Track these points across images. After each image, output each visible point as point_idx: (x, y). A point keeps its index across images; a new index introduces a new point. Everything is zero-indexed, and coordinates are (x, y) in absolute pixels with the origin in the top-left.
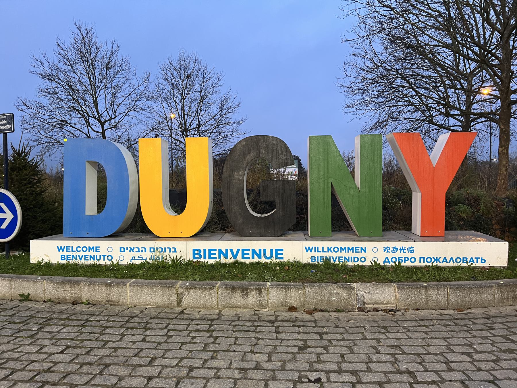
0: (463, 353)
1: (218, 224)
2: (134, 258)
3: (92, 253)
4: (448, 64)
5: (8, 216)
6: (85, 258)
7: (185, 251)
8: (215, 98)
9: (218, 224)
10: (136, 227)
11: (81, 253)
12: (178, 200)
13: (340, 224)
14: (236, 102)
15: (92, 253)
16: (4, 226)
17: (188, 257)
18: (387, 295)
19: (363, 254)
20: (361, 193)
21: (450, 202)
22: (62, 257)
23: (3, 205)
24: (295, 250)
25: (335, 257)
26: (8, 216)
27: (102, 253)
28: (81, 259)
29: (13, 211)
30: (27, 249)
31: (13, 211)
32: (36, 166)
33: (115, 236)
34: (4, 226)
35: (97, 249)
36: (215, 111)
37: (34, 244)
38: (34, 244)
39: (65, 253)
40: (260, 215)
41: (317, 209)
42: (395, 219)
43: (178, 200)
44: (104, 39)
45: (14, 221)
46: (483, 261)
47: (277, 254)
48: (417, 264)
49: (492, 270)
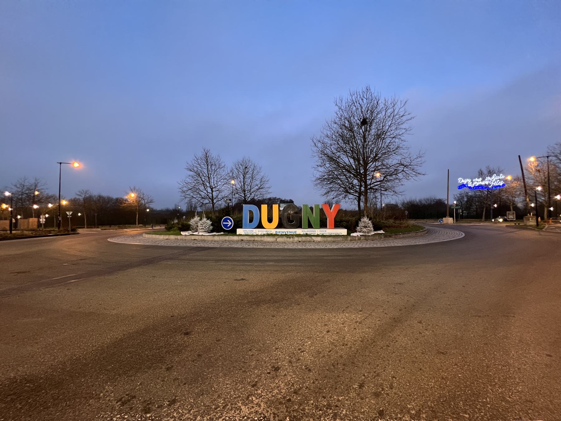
1: (280, 226)
4: (268, 266)
5: (230, 223)
7: (274, 231)
8: (258, 177)
9: (280, 226)
10: (260, 226)
12: (270, 220)
13: (310, 226)
14: (268, 179)
17: (274, 233)
18: (319, 239)
20: (315, 217)
21: (335, 221)
24: (299, 231)
25: (309, 233)
26: (230, 223)
31: (231, 222)
33: (255, 228)
36: (258, 182)
37: (238, 230)
38: (238, 230)
41: (304, 222)
42: (323, 225)
43: (270, 220)
44: (213, 154)
45: (231, 225)
49: (343, 236)
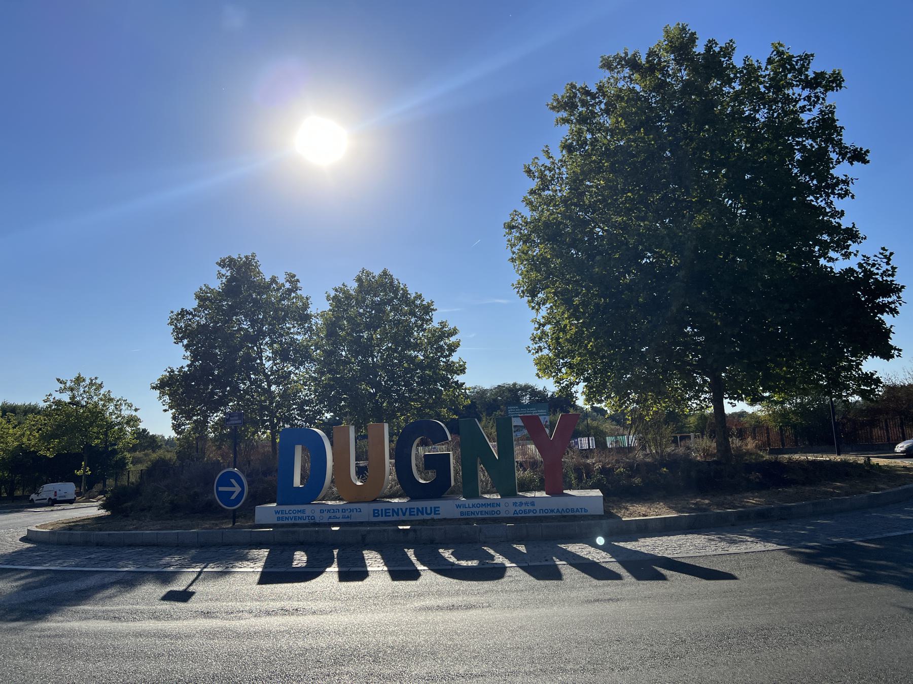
0: (439, 608)
2: (330, 517)
3: (300, 515)
5: (237, 489)
6: (410, 512)
11: (292, 515)
15: (300, 515)
16: (233, 497)
19: (498, 508)
22: (374, 513)
23: (233, 481)
26: (237, 489)
27: (307, 514)
28: (404, 514)
29: (242, 485)
30: (253, 512)
31: (242, 485)
32: (35, 452)
34: (233, 497)
35: (303, 511)
39: (280, 515)
40: (874, 461)
46: (586, 510)
47: (435, 511)
48: (538, 514)
